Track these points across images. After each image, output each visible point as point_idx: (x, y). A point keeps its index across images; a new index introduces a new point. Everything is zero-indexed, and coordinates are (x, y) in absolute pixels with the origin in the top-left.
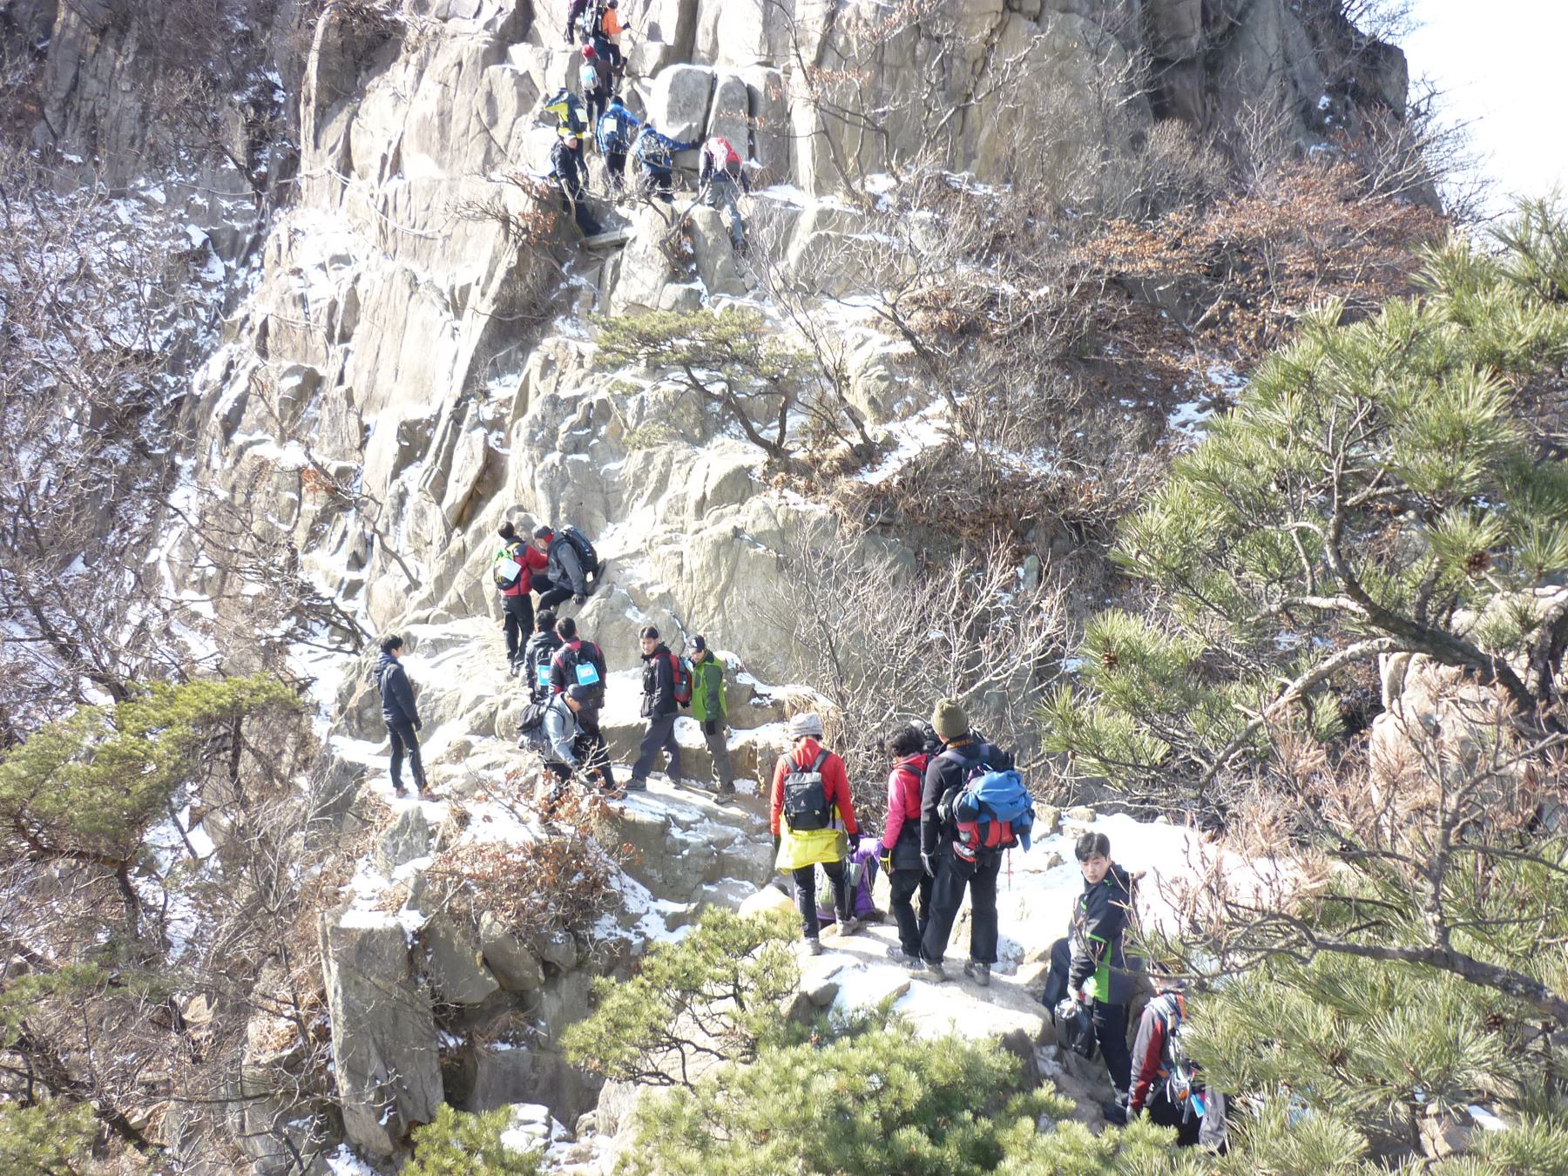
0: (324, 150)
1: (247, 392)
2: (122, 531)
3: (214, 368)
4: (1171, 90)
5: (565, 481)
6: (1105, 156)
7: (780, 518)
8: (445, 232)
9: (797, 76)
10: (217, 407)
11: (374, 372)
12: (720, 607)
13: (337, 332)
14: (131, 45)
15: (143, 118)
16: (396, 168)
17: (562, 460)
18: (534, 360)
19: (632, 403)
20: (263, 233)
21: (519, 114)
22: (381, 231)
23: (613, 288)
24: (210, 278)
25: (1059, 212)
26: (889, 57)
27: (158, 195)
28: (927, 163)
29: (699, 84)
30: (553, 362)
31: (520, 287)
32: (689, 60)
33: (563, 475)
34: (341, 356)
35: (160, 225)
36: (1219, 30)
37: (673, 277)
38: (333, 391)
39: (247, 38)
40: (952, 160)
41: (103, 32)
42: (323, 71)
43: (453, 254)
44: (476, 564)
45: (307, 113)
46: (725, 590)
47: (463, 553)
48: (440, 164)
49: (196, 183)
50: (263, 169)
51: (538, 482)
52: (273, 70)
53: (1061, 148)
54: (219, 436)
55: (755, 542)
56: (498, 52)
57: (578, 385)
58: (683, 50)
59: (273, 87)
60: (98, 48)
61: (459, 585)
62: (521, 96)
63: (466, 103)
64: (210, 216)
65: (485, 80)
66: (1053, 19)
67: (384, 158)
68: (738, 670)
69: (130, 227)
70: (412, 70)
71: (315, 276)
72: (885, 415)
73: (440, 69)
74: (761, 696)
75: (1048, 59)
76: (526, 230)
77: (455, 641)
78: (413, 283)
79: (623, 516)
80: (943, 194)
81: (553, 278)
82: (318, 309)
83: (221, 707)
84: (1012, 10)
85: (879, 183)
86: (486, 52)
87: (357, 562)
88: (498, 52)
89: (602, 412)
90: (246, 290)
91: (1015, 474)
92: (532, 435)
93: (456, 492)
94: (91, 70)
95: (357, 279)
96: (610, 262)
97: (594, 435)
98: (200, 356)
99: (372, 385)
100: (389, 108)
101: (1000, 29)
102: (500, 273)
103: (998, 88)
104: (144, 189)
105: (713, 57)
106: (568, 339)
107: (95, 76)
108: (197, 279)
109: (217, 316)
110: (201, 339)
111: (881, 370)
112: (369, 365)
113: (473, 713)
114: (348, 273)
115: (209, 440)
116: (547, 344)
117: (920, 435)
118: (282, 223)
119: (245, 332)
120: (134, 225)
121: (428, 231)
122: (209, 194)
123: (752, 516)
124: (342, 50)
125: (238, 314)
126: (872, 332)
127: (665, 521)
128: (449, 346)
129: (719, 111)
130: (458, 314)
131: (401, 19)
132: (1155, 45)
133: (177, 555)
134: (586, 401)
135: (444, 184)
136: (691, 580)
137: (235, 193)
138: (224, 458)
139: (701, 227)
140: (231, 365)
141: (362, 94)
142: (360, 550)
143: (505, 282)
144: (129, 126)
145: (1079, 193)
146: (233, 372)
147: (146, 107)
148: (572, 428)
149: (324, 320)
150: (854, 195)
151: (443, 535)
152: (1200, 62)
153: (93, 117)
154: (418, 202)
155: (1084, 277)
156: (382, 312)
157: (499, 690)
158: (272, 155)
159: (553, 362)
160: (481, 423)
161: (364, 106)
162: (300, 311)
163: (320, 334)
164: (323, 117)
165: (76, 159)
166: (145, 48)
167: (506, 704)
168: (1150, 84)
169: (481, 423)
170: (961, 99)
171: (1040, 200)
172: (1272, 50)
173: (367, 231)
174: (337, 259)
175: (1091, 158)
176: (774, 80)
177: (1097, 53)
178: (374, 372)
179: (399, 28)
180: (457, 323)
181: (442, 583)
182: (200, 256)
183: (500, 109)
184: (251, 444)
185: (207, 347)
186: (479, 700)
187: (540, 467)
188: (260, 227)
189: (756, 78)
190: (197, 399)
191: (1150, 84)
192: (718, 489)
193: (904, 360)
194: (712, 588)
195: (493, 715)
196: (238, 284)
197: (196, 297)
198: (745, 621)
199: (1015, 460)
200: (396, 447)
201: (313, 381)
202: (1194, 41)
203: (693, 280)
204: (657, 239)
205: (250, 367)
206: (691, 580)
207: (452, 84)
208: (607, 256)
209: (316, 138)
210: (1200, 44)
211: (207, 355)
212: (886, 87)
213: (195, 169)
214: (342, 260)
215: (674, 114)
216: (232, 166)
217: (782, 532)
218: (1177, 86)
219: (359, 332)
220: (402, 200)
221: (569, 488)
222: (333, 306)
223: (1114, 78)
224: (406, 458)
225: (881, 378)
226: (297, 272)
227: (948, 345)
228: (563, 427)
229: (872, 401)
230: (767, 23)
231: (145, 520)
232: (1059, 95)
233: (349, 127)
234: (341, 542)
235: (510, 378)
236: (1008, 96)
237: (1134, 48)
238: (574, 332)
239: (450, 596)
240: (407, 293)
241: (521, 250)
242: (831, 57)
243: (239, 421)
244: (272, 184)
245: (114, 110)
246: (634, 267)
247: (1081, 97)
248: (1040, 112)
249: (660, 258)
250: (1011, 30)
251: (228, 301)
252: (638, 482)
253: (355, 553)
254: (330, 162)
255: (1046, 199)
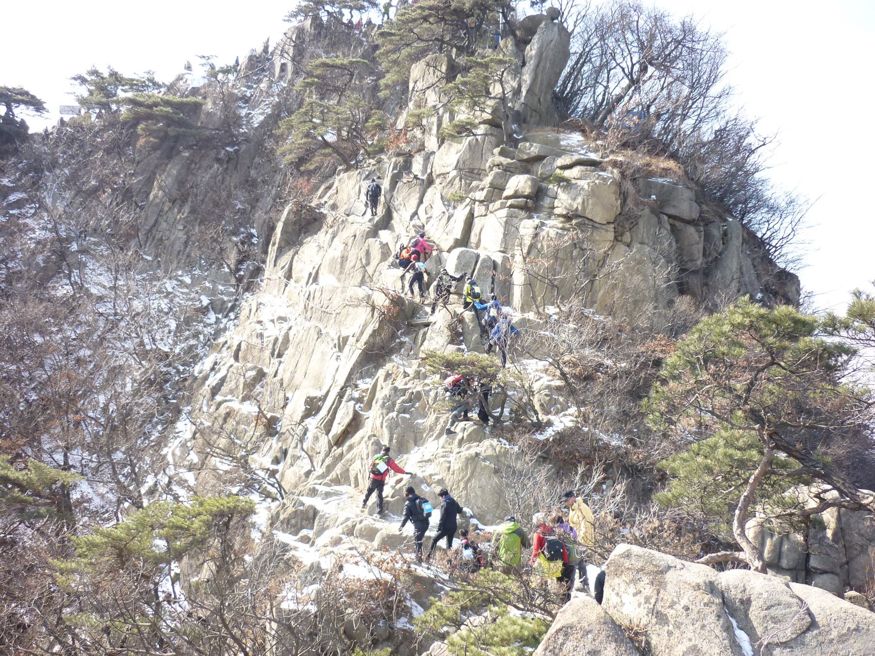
0: (278, 267)
1: (226, 376)
2: (145, 439)
3: (207, 364)
4: (687, 283)
5: (397, 425)
6: (655, 308)
7: (498, 449)
8: (337, 311)
9: (519, 258)
10: (207, 383)
11: (294, 373)
12: (465, 488)
13: (276, 353)
14: (186, 209)
15: (186, 243)
16: (315, 280)
17: (397, 416)
18: (381, 373)
19: (432, 394)
20: (237, 303)
21: (381, 262)
22: (305, 308)
23: (422, 344)
24: (208, 321)
25: (633, 330)
26: (560, 255)
27: (188, 280)
28: (575, 302)
29: (472, 257)
30: (391, 374)
31: (378, 338)
32: (466, 246)
33: (397, 422)
34: (277, 364)
35: (187, 294)
36: (710, 259)
37: (452, 342)
38: (268, 379)
39: (243, 212)
40: (586, 303)
41: (174, 202)
42: (283, 232)
43: (340, 322)
44: (348, 461)
45: (272, 250)
46: (469, 480)
47: (341, 455)
48: (339, 280)
49: (207, 276)
50: (242, 273)
51: (385, 424)
52: (254, 228)
53: (636, 303)
54: (208, 396)
55: (485, 459)
56: (373, 233)
57: (406, 384)
58: (464, 241)
59: (252, 236)
60: (170, 209)
61: (338, 470)
62: (382, 253)
63: (355, 255)
64: (212, 293)
65: (366, 244)
66: (636, 247)
67: (310, 274)
68: (471, 517)
69: (172, 293)
70: (329, 236)
71: (269, 325)
72: (548, 413)
73: (345, 237)
74: (480, 530)
75: (633, 263)
76: (384, 313)
77: (336, 494)
78: (320, 333)
79: (423, 444)
80: (582, 318)
81: (393, 336)
82: (268, 342)
83: (229, 508)
84: (618, 241)
85: (551, 310)
86: (368, 232)
87: (276, 461)
88: (373, 233)
89: (418, 396)
90: (225, 329)
91: (604, 443)
92: (384, 403)
93: (337, 429)
94: (165, 218)
95: (290, 328)
96: (422, 332)
97: (413, 406)
98: (196, 359)
99: (292, 379)
100: (312, 252)
101: (612, 248)
102: (369, 331)
103: (609, 274)
104: (181, 276)
105: (478, 246)
106: (395, 364)
107: (166, 221)
108: (201, 321)
109: (209, 340)
110: (200, 351)
111: (547, 392)
112: (291, 369)
113: (344, 525)
114: (286, 326)
115: (201, 398)
116: (389, 366)
117: (562, 421)
118: (249, 301)
119: (224, 349)
120: (176, 290)
121: (328, 310)
122: (213, 282)
123: (485, 448)
124: (295, 223)
125: (221, 340)
126: (543, 375)
127: (443, 447)
128: (334, 364)
129: (479, 269)
130: (341, 349)
131: (325, 212)
132: (681, 262)
133: (178, 452)
134: (410, 391)
135: (340, 289)
136: (453, 474)
137: (226, 283)
138: (209, 406)
139: (467, 320)
140: (216, 364)
141: (301, 244)
142: (279, 455)
143: (371, 336)
144: (178, 246)
145: (643, 323)
146: (217, 367)
147: (188, 238)
148: (403, 402)
149: (271, 346)
150: (539, 313)
151: (327, 449)
152: (701, 272)
153: (161, 240)
154: (326, 296)
155: (642, 359)
156: (302, 345)
157: (357, 516)
158: (248, 267)
159: (391, 374)
160: (352, 399)
161: (302, 249)
162: (259, 341)
163: (267, 353)
164: (280, 252)
165: (149, 258)
166: (193, 211)
167: (361, 522)
168: (678, 279)
169: (352, 399)
170: (592, 277)
171: (624, 324)
172: (734, 270)
173: (296, 307)
174: (280, 318)
175: (649, 308)
176: (505, 259)
177: (654, 263)
178: (294, 373)
179: (324, 216)
180: (339, 354)
181: (329, 469)
182: (204, 311)
183: (372, 258)
184: (226, 401)
185: (202, 354)
186: (348, 519)
187: (386, 418)
188: (236, 300)
189: (498, 258)
190: (196, 378)
191: (678, 279)
192: (469, 435)
193: (558, 389)
194: (463, 478)
195: (354, 526)
196: (222, 326)
197: (200, 328)
198: (477, 495)
199: (605, 438)
200: (303, 408)
201: (261, 375)
202: (699, 263)
203: (461, 344)
204: (446, 324)
205: (228, 365)
206: (453, 474)
207: (350, 244)
208: (419, 329)
209: (275, 262)
210: (702, 264)
211: (201, 359)
212: (558, 268)
213: (208, 270)
214: (283, 319)
215: (457, 269)
216: (227, 270)
217: (497, 456)
218: (690, 281)
219: (288, 353)
220: (318, 294)
221: (399, 429)
222: (276, 340)
223: (661, 275)
224: (308, 414)
225: (546, 395)
226: (260, 322)
227: (577, 384)
228: (399, 401)
229: (542, 405)
230: (505, 235)
231: (157, 434)
232: (637, 279)
233: (293, 258)
234: (268, 451)
235: (368, 380)
236: (613, 278)
237: (672, 263)
238: (401, 362)
239: (333, 475)
240: (316, 337)
241: (381, 322)
242: (534, 252)
243: (219, 389)
244: (245, 281)
245: (172, 238)
246: (433, 335)
247: (647, 281)
248: (628, 286)
249: (447, 332)
250: (616, 249)
251: (215, 334)
252: (431, 429)
253: (276, 457)
254: (281, 273)
255: (628, 324)
